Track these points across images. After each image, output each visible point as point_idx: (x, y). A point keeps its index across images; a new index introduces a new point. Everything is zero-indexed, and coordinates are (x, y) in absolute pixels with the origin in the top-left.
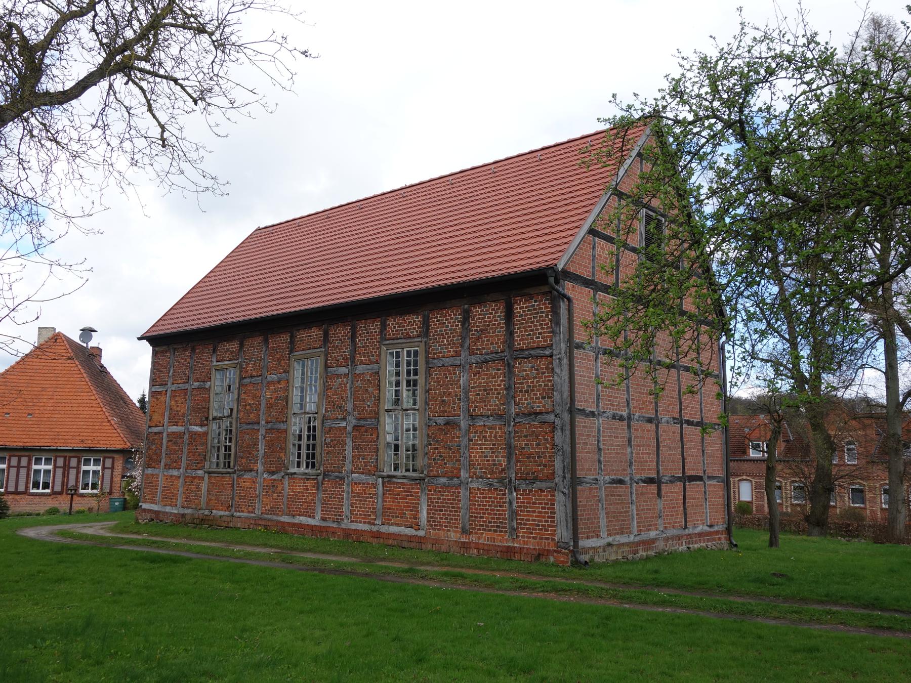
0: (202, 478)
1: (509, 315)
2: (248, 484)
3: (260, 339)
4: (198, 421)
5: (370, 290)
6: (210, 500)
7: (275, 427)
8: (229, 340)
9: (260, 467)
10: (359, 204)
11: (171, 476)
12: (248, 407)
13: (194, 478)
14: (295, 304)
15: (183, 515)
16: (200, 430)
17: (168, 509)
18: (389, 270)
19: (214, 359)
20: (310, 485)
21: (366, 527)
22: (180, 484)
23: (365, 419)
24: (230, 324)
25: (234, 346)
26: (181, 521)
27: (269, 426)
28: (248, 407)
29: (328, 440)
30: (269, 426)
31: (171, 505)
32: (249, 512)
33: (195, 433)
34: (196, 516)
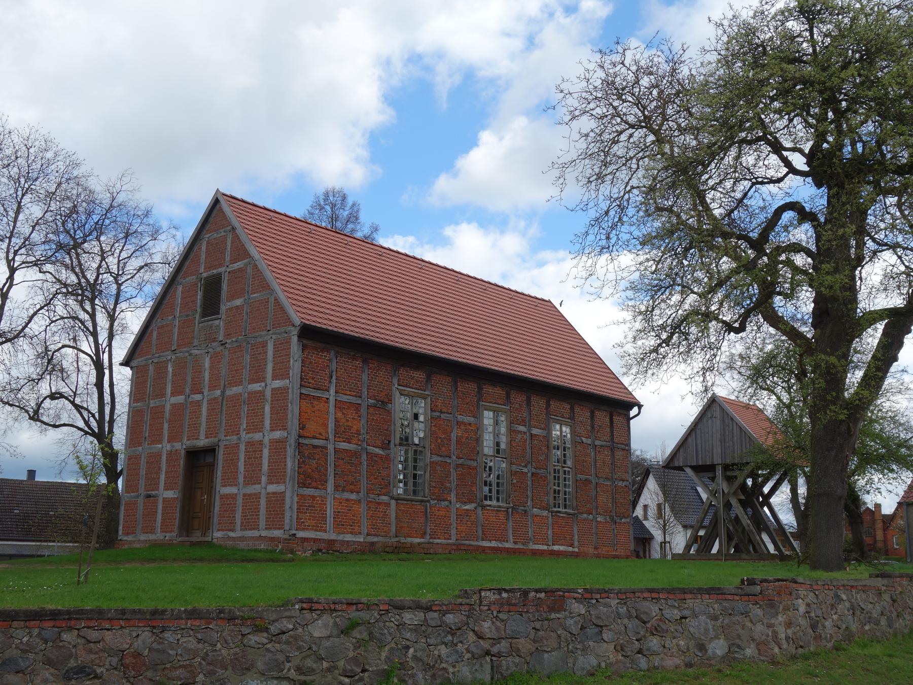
0: (547, 517)
1: (592, 417)
2: (442, 513)
3: (449, 379)
4: (379, 443)
5: (480, 360)
6: (401, 527)
7: (466, 463)
8: (417, 368)
9: (453, 497)
10: (460, 276)
11: (347, 500)
12: (439, 441)
13: (379, 504)
14: (401, 341)
15: (373, 544)
16: (381, 452)
17: (349, 538)
18: (374, 313)
19: (395, 381)
20: (502, 516)
21: (545, 547)
22: (363, 509)
23: (540, 469)
24: (396, 347)
25: (419, 375)
26: (368, 551)
27: (461, 461)
28: (439, 441)
29: (515, 481)
30: (461, 461)
31: (352, 533)
32: (445, 539)
33: (376, 455)
34: (390, 544)
